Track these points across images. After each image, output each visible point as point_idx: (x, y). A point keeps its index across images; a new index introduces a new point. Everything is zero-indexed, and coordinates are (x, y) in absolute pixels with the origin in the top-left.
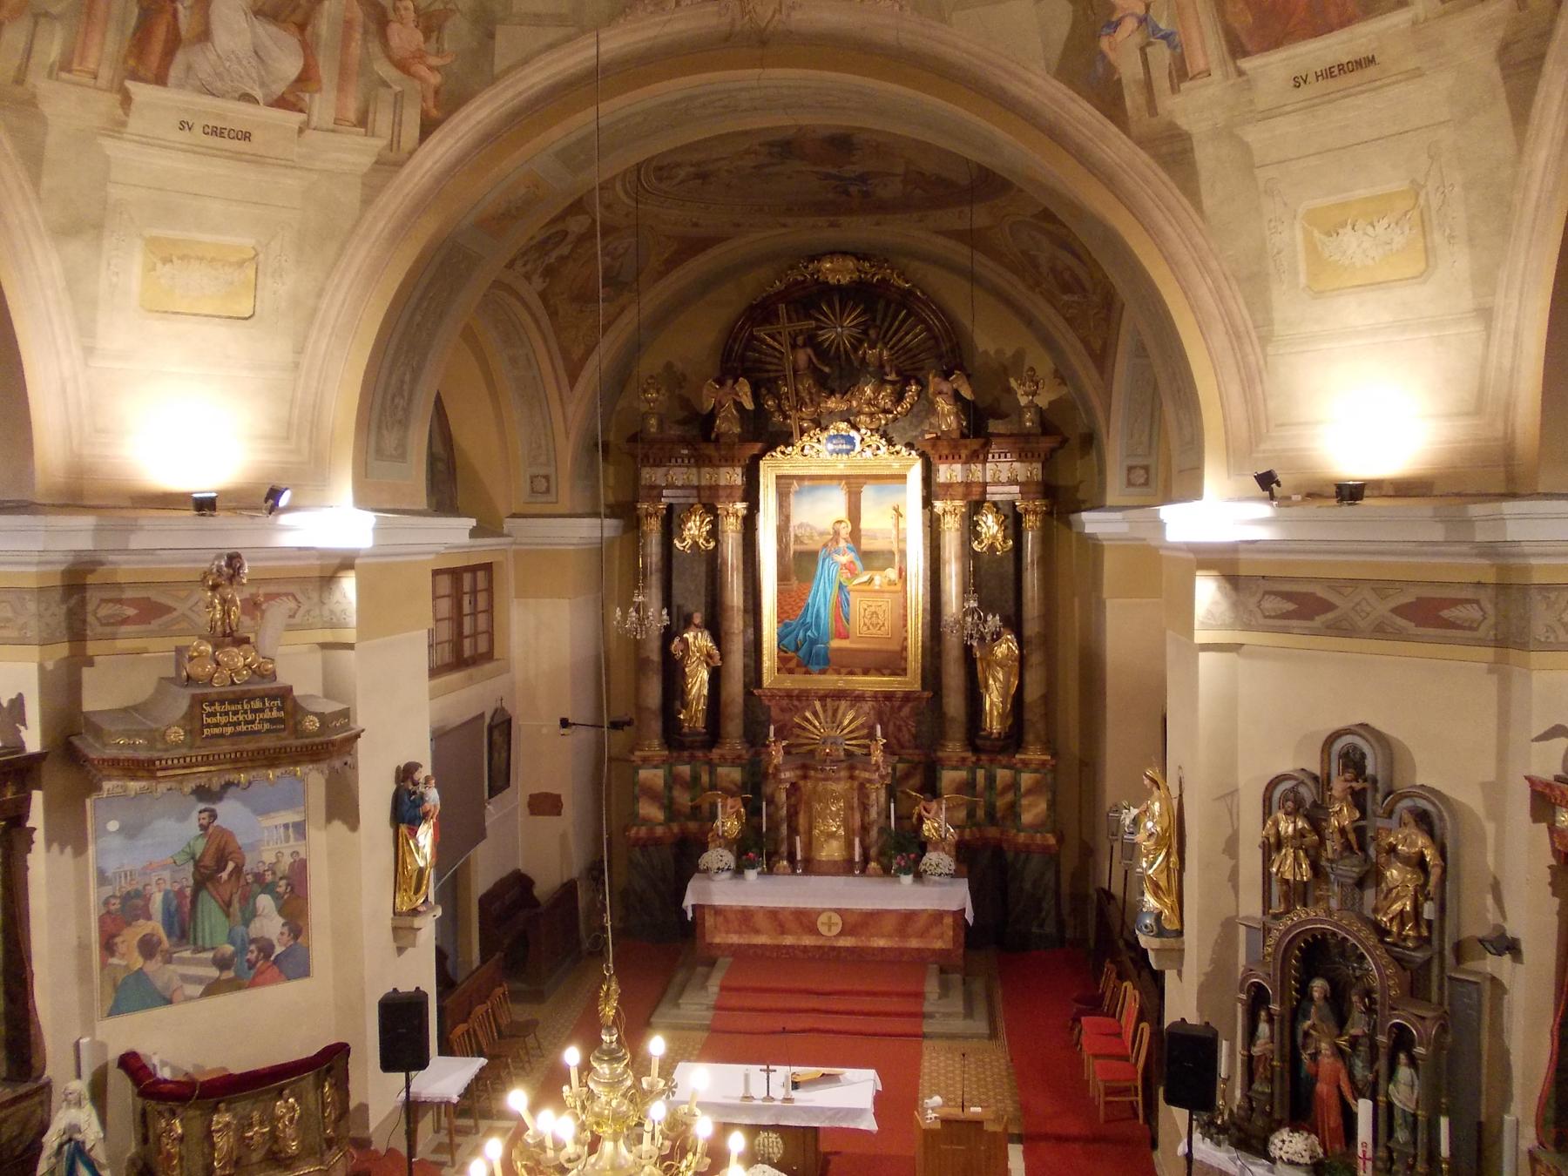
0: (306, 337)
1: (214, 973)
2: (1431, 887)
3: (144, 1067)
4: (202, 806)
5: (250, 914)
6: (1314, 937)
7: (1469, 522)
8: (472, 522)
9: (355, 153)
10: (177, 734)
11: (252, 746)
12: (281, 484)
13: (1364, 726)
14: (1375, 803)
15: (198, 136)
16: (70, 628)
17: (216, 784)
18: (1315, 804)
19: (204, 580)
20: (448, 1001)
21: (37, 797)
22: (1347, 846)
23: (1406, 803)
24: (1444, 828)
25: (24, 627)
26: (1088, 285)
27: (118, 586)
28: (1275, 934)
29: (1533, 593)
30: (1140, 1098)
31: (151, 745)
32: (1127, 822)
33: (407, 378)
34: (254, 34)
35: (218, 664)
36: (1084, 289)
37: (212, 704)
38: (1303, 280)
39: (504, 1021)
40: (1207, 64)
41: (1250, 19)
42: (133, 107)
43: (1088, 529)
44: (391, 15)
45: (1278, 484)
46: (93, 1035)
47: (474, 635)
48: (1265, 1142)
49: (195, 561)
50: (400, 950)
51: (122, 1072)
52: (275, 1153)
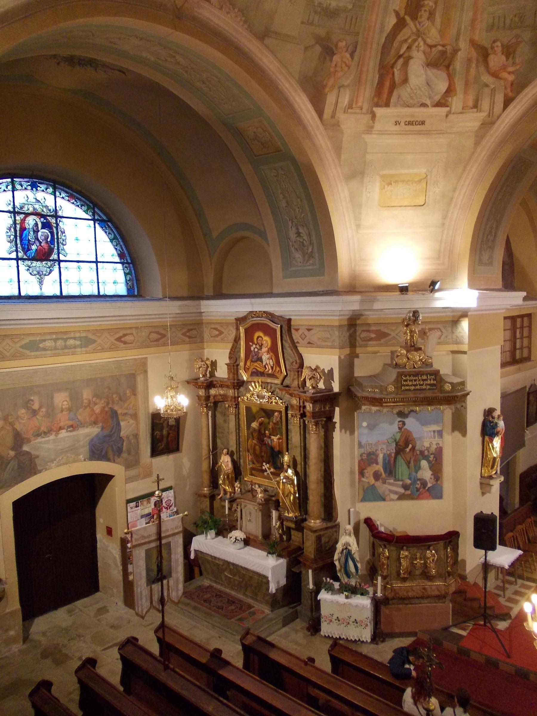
0: (448, 212)
1: (402, 491)
3: (374, 525)
4: (399, 419)
5: (418, 468)
8: (524, 294)
9: (472, 121)
10: (391, 388)
11: (422, 395)
12: (436, 279)
15: (402, 126)
16: (350, 342)
17: (406, 410)
19: (403, 322)
20: (504, 521)
21: (337, 410)
25: (333, 341)
27: (369, 325)
31: (381, 392)
33: (494, 226)
34: (427, 75)
35: (408, 359)
37: (406, 376)
39: (531, 535)
42: (376, 119)
44: (490, 51)
46: (355, 507)
47: (522, 348)
49: (398, 314)
50: (483, 494)
51: (365, 525)
52: (425, 573)
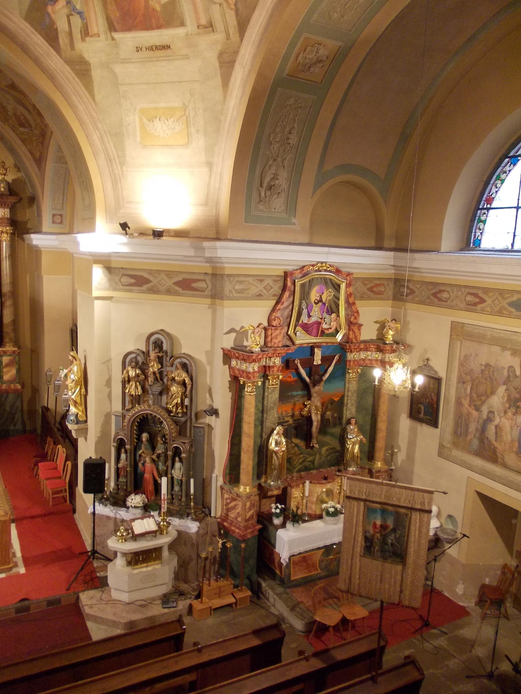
2: (188, 392)
6: (143, 417)
7: (203, 249)
13: (162, 330)
14: (167, 361)
18: (143, 363)
22: (156, 379)
23: (178, 360)
24: (192, 369)
26: (33, 125)
28: (128, 417)
29: (225, 277)
30: (68, 494)
32: (63, 376)
36: (31, 127)
38: (138, 139)
40: (98, 31)
41: (118, 14)
43: (35, 242)
45: (129, 228)
48: (125, 501)
